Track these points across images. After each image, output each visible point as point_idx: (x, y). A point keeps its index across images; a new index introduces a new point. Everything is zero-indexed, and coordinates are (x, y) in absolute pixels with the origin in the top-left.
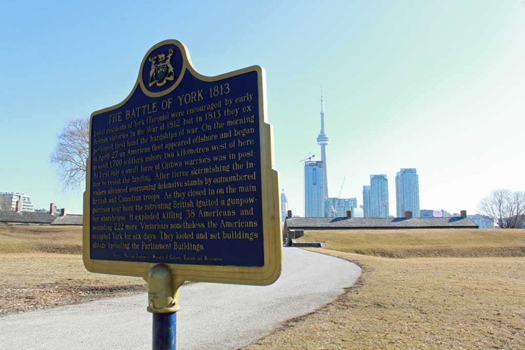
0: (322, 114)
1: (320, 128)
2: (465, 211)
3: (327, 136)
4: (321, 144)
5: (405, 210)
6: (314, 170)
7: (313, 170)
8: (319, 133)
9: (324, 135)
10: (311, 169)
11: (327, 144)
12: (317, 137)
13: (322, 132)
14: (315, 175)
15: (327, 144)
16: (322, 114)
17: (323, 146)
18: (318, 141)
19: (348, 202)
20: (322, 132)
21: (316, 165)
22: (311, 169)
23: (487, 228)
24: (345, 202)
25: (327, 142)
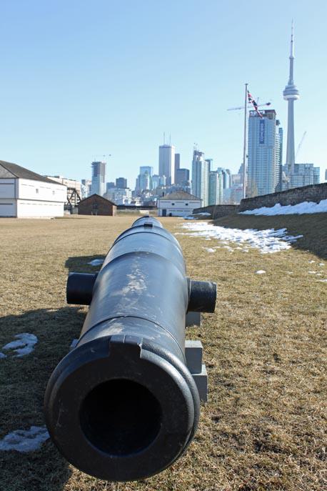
0: (292, 59)
1: (289, 78)
2: (312, 164)
3: (296, 88)
4: (288, 99)
5: (172, 147)
6: (262, 122)
7: (261, 123)
8: (287, 84)
9: (293, 87)
10: (257, 120)
11: (296, 99)
12: (284, 89)
13: (291, 82)
14: (262, 129)
15: (296, 99)
16: (292, 59)
17: (291, 101)
18: (284, 95)
19: (309, 168)
20: (291, 82)
21: (264, 116)
22: (257, 120)
23: (188, 184)
24: (306, 168)
25: (296, 96)
